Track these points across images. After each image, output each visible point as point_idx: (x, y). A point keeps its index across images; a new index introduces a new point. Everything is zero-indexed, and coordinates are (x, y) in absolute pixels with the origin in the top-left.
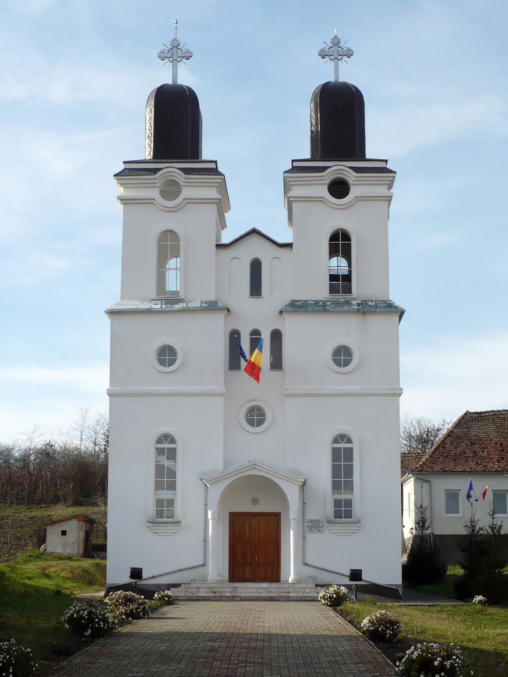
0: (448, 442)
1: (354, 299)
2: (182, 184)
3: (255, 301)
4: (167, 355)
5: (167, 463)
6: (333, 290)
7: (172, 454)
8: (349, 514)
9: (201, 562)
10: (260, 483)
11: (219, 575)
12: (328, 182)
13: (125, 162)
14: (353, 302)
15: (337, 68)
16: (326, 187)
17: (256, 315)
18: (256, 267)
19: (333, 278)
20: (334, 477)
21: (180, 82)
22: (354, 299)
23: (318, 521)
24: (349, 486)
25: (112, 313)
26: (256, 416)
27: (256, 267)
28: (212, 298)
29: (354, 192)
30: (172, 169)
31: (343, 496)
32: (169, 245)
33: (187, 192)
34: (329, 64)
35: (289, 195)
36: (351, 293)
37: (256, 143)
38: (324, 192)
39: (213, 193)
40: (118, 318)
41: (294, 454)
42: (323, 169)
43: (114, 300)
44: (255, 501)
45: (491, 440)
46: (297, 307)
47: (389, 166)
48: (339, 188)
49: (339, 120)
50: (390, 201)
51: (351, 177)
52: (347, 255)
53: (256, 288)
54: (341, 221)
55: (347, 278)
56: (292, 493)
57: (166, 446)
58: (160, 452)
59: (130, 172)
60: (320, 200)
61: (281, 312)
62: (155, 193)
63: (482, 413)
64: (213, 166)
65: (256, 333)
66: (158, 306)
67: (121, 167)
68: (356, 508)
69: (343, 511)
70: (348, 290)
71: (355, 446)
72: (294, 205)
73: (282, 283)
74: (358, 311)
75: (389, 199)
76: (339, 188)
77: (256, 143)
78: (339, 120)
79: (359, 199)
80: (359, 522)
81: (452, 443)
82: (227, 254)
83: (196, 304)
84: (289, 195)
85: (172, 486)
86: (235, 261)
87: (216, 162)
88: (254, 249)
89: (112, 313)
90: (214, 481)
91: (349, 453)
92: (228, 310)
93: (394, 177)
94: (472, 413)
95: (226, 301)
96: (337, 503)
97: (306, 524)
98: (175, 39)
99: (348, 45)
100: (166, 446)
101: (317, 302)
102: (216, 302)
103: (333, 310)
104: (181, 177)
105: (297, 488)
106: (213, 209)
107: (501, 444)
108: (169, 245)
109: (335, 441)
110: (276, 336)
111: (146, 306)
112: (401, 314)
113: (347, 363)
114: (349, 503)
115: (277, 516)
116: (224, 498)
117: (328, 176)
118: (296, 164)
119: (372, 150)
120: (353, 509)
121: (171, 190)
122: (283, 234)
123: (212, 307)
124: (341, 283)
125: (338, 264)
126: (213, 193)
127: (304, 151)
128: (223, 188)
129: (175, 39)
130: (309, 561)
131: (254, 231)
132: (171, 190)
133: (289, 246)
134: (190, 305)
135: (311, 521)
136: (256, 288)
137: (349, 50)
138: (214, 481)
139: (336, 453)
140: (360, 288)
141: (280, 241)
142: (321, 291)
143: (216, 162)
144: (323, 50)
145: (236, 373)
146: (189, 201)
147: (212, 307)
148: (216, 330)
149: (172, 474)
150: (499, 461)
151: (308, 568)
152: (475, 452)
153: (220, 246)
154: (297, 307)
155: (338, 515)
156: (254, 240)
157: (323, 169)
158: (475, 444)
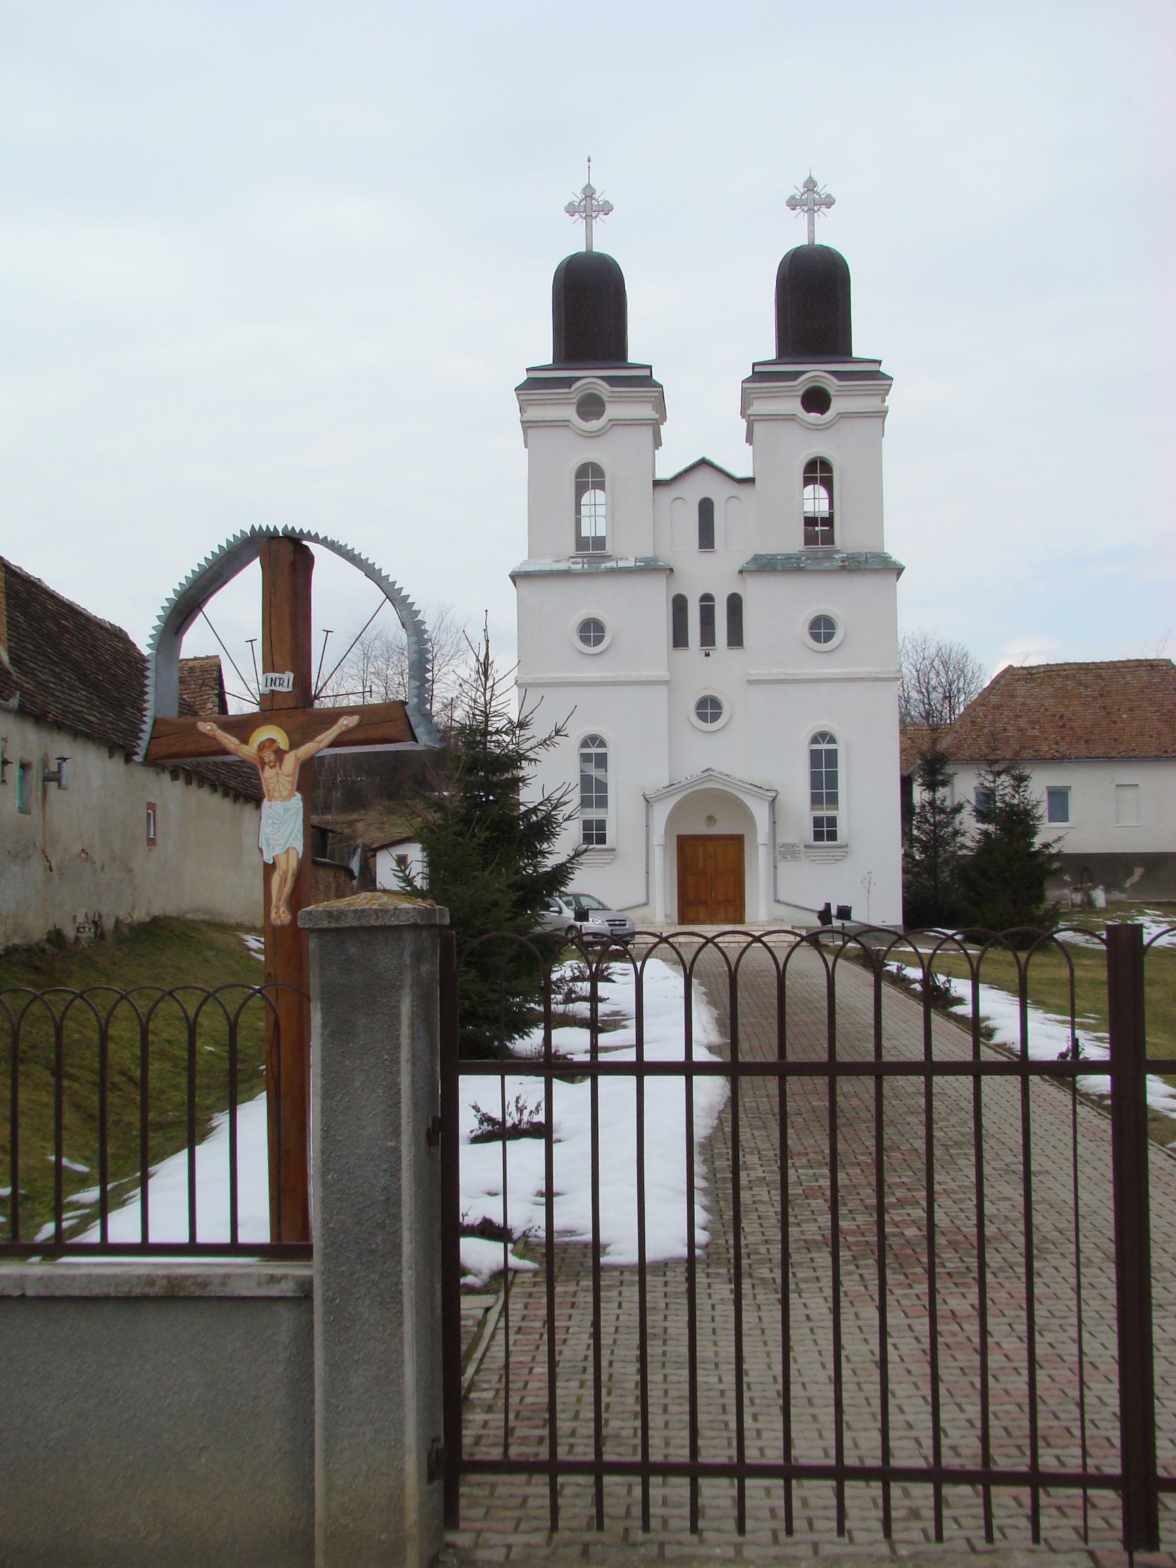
0: (981, 711)
1: (838, 552)
2: (605, 399)
3: (707, 558)
4: (592, 631)
5: (595, 773)
6: (810, 539)
7: (601, 761)
8: (832, 836)
9: (642, 900)
10: (711, 796)
11: (666, 916)
12: (801, 393)
13: (528, 370)
14: (837, 556)
15: (811, 223)
16: (799, 399)
17: (709, 575)
18: (706, 508)
19: (810, 521)
20: (813, 787)
21: (597, 249)
22: (838, 552)
23: (793, 845)
24: (833, 800)
25: (515, 577)
26: (709, 708)
27: (706, 508)
28: (648, 553)
29: (837, 406)
30: (591, 379)
31: (825, 813)
32: (589, 477)
33: (612, 411)
34: (800, 219)
35: (749, 412)
36: (833, 543)
37: (702, 332)
38: (794, 406)
39: (646, 411)
40: (524, 585)
41: (761, 758)
42: (796, 375)
43: (519, 558)
44: (711, 819)
45: (1046, 710)
46: (764, 566)
47: (882, 369)
48: (816, 400)
49: (813, 300)
50: (884, 417)
51: (832, 385)
52: (828, 484)
53: (706, 539)
54: (818, 447)
55: (828, 521)
56: (760, 812)
57: (593, 750)
58: (585, 758)
59: (535, 385)
60: (790, 418)
61: (741, 572)
62: (569, 413)
63: (1031, 668)
64: (646, 373)
65: (707, 598)
66: (579, 567)
67: (523, 377)
68: (841, 828)
69: (825, 830)
70: (829, 539)
71: (840, 747)
72: (757, 427)
73: (741, 534)
74: (843, 569)
75: (882, 414)
76: (816, 400)
77: (702, 332)
78: (813, 300)
79: (843, 416)
80: (847, 846)
81: (985, 716)
82: (666, 495)
83: (630, 563)
84: (749, 412)
85: (602, 803)
86: (679, 502)
87: (650, 367)
88: (703, 486)
89: (515, 577)
90: (661, 797)
91: (832, 756)
92: (671, 570)
93: (890, 385)
94: (1018, 669)
95: (667, 557)
96: (817, 822)
97: (778, 849)
98: (589, 186)
99: (828, 190)
100: (593, 750)
101: (788, 557)
102: (655, 559)
103: (809, 568)
104: (604, 390)
105: (767, 805)
106: (648, 432)
107: (1062, 717)
108: (589, 477)
109: (815, 740)
110: (735, 604)
111: (563, 566)
112: (899, 571)
113: (829, 637)
114: (832, 821)
115: (738, 840)
116: (672, 819)
117: (801, 385)
118: (757, 369)
119: (861, 347)
120: (838, 829)
121: (591, 407)
122: (739, 462)
123: (650, 568)
124: (819, 530)
125: (815, 501)
126: (646, 411)
127: (768, 349)
128: (660, 404)
129: (589, 186)
130: (781, 897)
131: (703, 463)
132: (591, 407)
133: (750, 481)
134: (621, 564)
135: (784, 845)
136: (706, 539)
137: (829, 196)
138: (661, 797)
139: (815, 757)
140: (847, 538)
141: (739, 474)
142: (792, 541)
143: (650, 367)
144: (793, 198)
145: (681, 654)
146: (616, 423)
147: (650, 568)
148: (654, 600)
149: (602, 786)
150: (1057, 743)
151: (780, 907)
152: (1020, 730)
153: (657, 484)
154: (764, 566)
155: (818, 836)
156: (704, 474)
157: (796, 375)
158: (1021, 717)
